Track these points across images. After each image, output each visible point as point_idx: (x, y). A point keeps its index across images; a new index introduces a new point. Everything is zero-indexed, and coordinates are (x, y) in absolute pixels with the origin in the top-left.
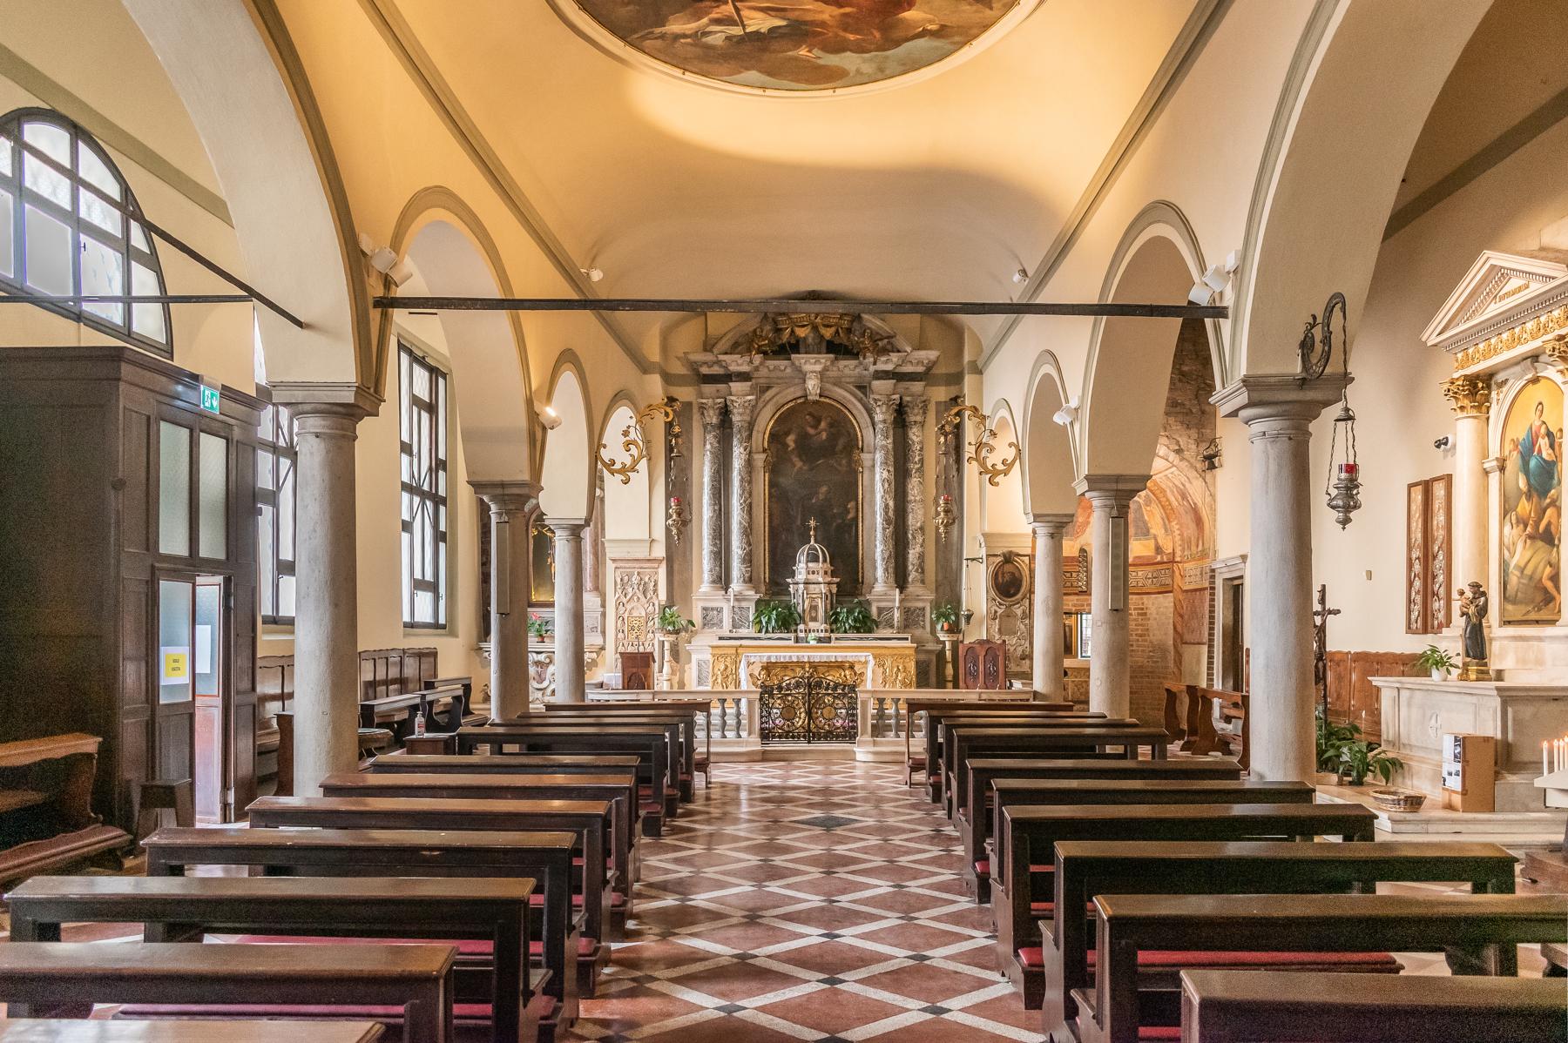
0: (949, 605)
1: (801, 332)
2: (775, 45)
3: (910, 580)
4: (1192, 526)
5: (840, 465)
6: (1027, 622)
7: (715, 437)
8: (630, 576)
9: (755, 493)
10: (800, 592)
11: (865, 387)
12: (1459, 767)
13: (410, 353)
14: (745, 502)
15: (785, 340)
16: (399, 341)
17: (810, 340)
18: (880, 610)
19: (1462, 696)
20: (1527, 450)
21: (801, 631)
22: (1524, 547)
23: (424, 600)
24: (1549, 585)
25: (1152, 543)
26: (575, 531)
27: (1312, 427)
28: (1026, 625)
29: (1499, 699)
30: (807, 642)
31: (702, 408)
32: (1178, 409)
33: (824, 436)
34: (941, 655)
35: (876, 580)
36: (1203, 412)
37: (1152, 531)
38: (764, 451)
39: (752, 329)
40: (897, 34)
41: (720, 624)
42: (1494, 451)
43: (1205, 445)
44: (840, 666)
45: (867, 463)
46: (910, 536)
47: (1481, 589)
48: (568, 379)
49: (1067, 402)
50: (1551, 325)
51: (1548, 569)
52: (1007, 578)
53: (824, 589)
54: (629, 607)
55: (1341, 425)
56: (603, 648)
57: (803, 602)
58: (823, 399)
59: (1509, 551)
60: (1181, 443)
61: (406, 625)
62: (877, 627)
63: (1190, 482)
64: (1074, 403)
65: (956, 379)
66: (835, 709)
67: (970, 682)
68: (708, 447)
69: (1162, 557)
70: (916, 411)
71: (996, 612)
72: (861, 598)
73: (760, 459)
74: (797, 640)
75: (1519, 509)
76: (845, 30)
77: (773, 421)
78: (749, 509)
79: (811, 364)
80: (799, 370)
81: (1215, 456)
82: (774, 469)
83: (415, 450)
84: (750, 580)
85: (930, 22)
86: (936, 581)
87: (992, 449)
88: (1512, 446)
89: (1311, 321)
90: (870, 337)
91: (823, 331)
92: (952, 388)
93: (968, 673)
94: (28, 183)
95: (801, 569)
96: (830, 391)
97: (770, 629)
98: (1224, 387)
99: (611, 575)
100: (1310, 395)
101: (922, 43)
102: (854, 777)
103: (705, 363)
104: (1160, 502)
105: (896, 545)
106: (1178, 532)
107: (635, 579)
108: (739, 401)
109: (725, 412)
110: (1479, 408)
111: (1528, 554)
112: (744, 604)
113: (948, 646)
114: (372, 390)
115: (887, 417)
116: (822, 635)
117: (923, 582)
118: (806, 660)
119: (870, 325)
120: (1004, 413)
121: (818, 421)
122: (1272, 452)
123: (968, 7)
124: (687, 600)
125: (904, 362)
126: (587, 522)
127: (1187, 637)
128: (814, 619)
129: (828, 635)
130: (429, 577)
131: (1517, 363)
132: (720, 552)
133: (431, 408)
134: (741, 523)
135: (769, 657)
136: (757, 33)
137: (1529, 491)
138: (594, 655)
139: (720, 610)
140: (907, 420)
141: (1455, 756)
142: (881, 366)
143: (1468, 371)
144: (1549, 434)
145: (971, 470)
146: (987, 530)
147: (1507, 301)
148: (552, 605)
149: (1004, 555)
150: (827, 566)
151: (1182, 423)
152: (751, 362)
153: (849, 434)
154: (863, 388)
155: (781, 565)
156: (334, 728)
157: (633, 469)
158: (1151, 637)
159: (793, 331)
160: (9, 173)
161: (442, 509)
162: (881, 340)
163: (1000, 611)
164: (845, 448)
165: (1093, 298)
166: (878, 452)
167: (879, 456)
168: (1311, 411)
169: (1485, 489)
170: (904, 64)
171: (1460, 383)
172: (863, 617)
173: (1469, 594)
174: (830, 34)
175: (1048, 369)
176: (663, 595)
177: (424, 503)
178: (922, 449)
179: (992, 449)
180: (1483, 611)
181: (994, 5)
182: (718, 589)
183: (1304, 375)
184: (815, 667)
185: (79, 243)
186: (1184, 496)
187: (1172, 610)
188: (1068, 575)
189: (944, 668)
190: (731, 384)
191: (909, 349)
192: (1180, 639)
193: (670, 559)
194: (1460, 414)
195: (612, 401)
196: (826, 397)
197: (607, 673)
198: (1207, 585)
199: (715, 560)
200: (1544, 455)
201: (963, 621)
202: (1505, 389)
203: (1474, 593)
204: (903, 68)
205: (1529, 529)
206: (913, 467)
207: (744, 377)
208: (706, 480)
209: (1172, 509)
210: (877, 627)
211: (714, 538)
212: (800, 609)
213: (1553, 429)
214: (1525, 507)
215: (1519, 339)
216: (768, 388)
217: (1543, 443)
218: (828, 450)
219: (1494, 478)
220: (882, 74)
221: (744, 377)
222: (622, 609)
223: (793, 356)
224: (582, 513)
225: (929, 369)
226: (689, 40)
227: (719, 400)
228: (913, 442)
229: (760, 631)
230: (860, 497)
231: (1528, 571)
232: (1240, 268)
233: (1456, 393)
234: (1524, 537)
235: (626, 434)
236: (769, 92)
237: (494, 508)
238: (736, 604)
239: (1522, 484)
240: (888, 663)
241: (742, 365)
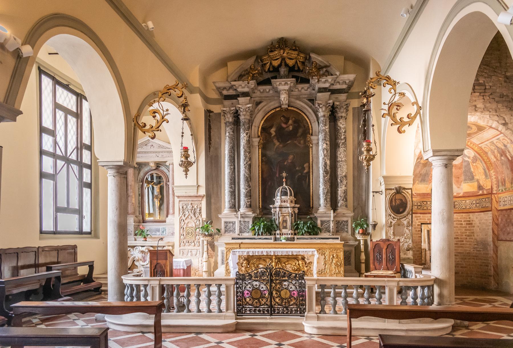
3: (339, 205)
5: (300, 143)
6: (410, 228)
7: (231, 129)
10: (277, 212)
11: (313, 100)
14: (247, 163)
18: (322, 222)
21: (278, 234)
25: (476, 184)
28: (409, 230)
30: (281, 241)
32: (504, 99)
33: (291, 128)
34: (358, 247)
35: (320, 205)
37: (476, 177)
38: (259, 137)
41: (234, 231)
44: (295, 258)
45: (314, 142)
52: (398, 202)
53: (290, 210)
54: (186, 222)
58: (290, 108)
60: (506, 119)
62: (321, 232)
66: (290, 291)
67: (377, 264)
68: (227, 134)
69: (483, 192)
70: (342, 110)
71: (391, 222)
72: (312, 216)
73: (256, 141)
74: (276, 239)
77: (263, 121)
78: (249, 167)
79: (282, 85)
82: (264, 147)
84: (250, 206)
86: (354, 206)
95: (278, 200)
96: (294, 103)
97: (260, 233)
103: (224, 88)
105: (331, 186)
106: (495, 177)
107: (190, 207)
108: (243, 107)
109: (236, 115)
112: (246, 220)
113: (362, 242)
115: (326, 114)
116: (289, 236)
117: (346, 206)
118: (272, 254)
121: (287, 120)
127: (502, 237)
128: (285, 228)
129: (292, 236)
132: (234, 191)
134: (245, 175)
135: (248, 252)
139: (234, 223)
140: (337, 116)
146: (385, 174)
149: (396, 189)
150: (292, 198)
153: (305, 126)
154: (312, 101)
158: (476, 236)
159: (271, 63)
163: (394, 222)
164: (302, 134)
166: (320, 133)
167: (321, 136)
172: (313, 226)
176: (204, 215)
178: (345, 132)
182: (232, 212)
184: (279, 259)
187: (491, 221)
188: (425, 203)
189: (360, 255)
191: (338, 73)
192: (497, 238)
193: (209, 196)
196: (292, 107)
199: (231, 195)
201: (371, 227)
206: (341, 142)
207: (245, 94)
208: (227, 152)
209: (491, 163)
210: (321, 232)
212: (277, 222)
216: (260, 102)
218: (293, 135)
221: (245, 94)
222: (183, 223)
227: (232, 108)
228: (340, 128)
229: (255, 235)
230: (311, 160)
238: (242, 220)
240: (327, 253)
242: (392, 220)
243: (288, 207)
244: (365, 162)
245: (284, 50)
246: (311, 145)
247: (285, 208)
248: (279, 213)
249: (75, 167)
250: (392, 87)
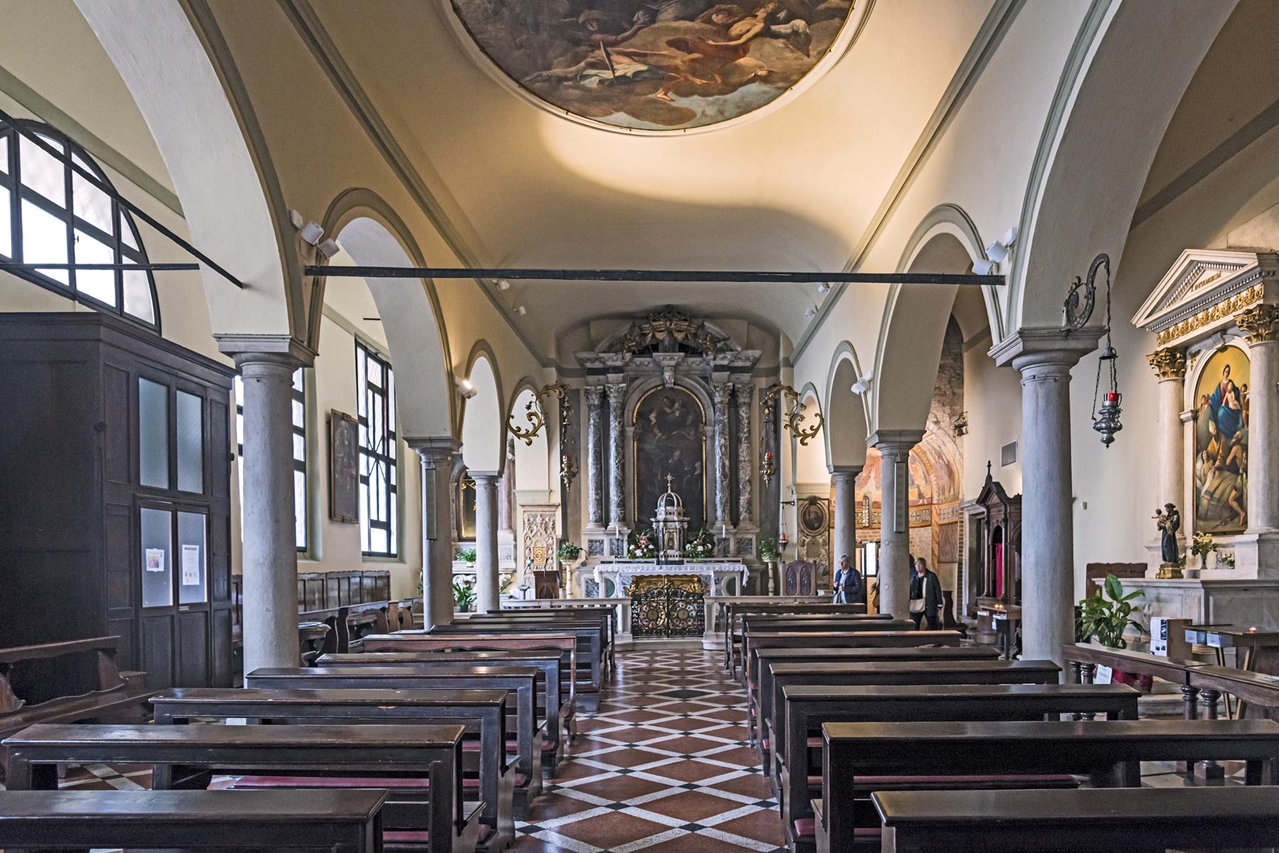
0: (772, 541)
1: (660, 336)
2: (639, 88)
3: (741, 518)
4: (946, 478)
5: (689, 435)
8: (535, 517)
9: (627, 456)
10: (661, 528)
12: (1165, 643)
13: (365, 349)
15: (648, 342)
16: (356, 340)
17: (667, 343)
19: (1170, 589)
20: (1216, 401)
22: (1213, 478)
23: (379, 535)
24: (1235, 504)
26: (492, 481)
27: (1072, 371)
29: (1203, 591)
31: (587, 392)
33: (677, 414)
35: (716, 519)
36: (954, 394)
37: (916, 482)
38: (633, 425)
39: (623, 334)
40: (735, 79)
42: (1189, 404)
43: (955, 418)
45: (709, 434)
46: (741, 487)
47: (1175, 509)
48: (482, 363)
49: (861, 375)
50: (1239, 303)
51: (1234, 493)
53: (677, 525)
55: (1106, 363)
56: (515, 571)
57: (663, 535)
58: (676, 387)
59: (1200, 480)
61: (364, 554)
63: (945, 445)
64: (867, 377)
65: (775, 371)
68: (592, 421)
70: (745, 395)
73: (630, 430)
75: (1209, 448)
76: (694, 75)
80: (658, 365)
81: (963, 426)
82: (640, 438)
84: (623, 520)
85: (761, 68)
87: (802, 418)
88: (1203, 401)
89: (1077, 281)
90: (711, 340)
91: (676, 335)
92: (771, 378)
93: (787, 584)
94: (25, 181)
98: (1001, 341)
99: (520, 515)
100: (1072, 344)
101: (754, 87)
102: (702, 661)
103: (588, 360)
104: (922, 461)
107: (539, 520)
109: (604, 396)
110: (1176, 373)
111: (1216, 483)
114: (305, 343)
117: (750, 520)
119: (710, 331)
120: (811, 393)
121: (673, 402)
122: (1041, 392)
123: (791, 55)
124: (578, 535)
125: (737, 358)
126: (501, 473)
128: (672, 548)
129: (681, 559)
130: (383, 518)
131: (1209, 337)
132: (601, 499)
133: (384, 393)
134: (616, 478)
136: (624, 76)
137: (1218, 433)
138: (509, 576)
141: (1162, 635)
142: (719, 362)
143: (1169, 345)
144: (1235, 389)
145: (786, 434)
147: (1201, 288)
148: (474, 540)
151: (939, 401)
152: (623, 358)
155: (647, 509)
156: (276, 623)
157: (534, 434)
159: (653, 335)
160: (6, 171)
161: (393, 468)
162: (719, 342)
163: (807, 540)
164: (693, 422)
165: (891, 270)
168: (1073, 358)
169: (1182, 435)
170: (739, 107)
171: (1163, 354)
173: (1165, 513)
174: (682, 79)
175: (847, 355)
177: (378, 463)
179: (802, 418)
180: (1177, 525)
181: (811, 53)
183: (1068, 327)
185: (73, 235)
186: (940, 456)
187: (930, 539)
189: (768, 582)
190: (609, 375)
191: (739, 349)
193: (564, 504)
194: (1162, 379)
195: (519, 383)
197: (519, 593)
200: (1231, 406)
202: (1198, 358)
203: (1169, 512)
204: (738, 110)
205: (1217, 463)
206: (743, 436)
207: (617, 370)
208: (591, 446)
209: (931, 466)
211: (597, 489)
213: (1239, 385)
214: (1213, 446)
215: (1212, 317)
216: (636, 378)
217: (1230, 396)
218: (680, 424)
219: (1189, 427)
220: (722, 116)
221: (617, 370)
222: (528, 542)
223: (654, 354)
224: (495, 467)
225: (754, 364)
226: (570, 83)
231: (1217, 495)
232: (1017, 243)
233: (1159, 362)
234: (1213, 469)
235: (529, 407)
236: (634, 132)
237: (423, 457)
239: (1212, 429)
241: (617, 360)
243: (675, 521)
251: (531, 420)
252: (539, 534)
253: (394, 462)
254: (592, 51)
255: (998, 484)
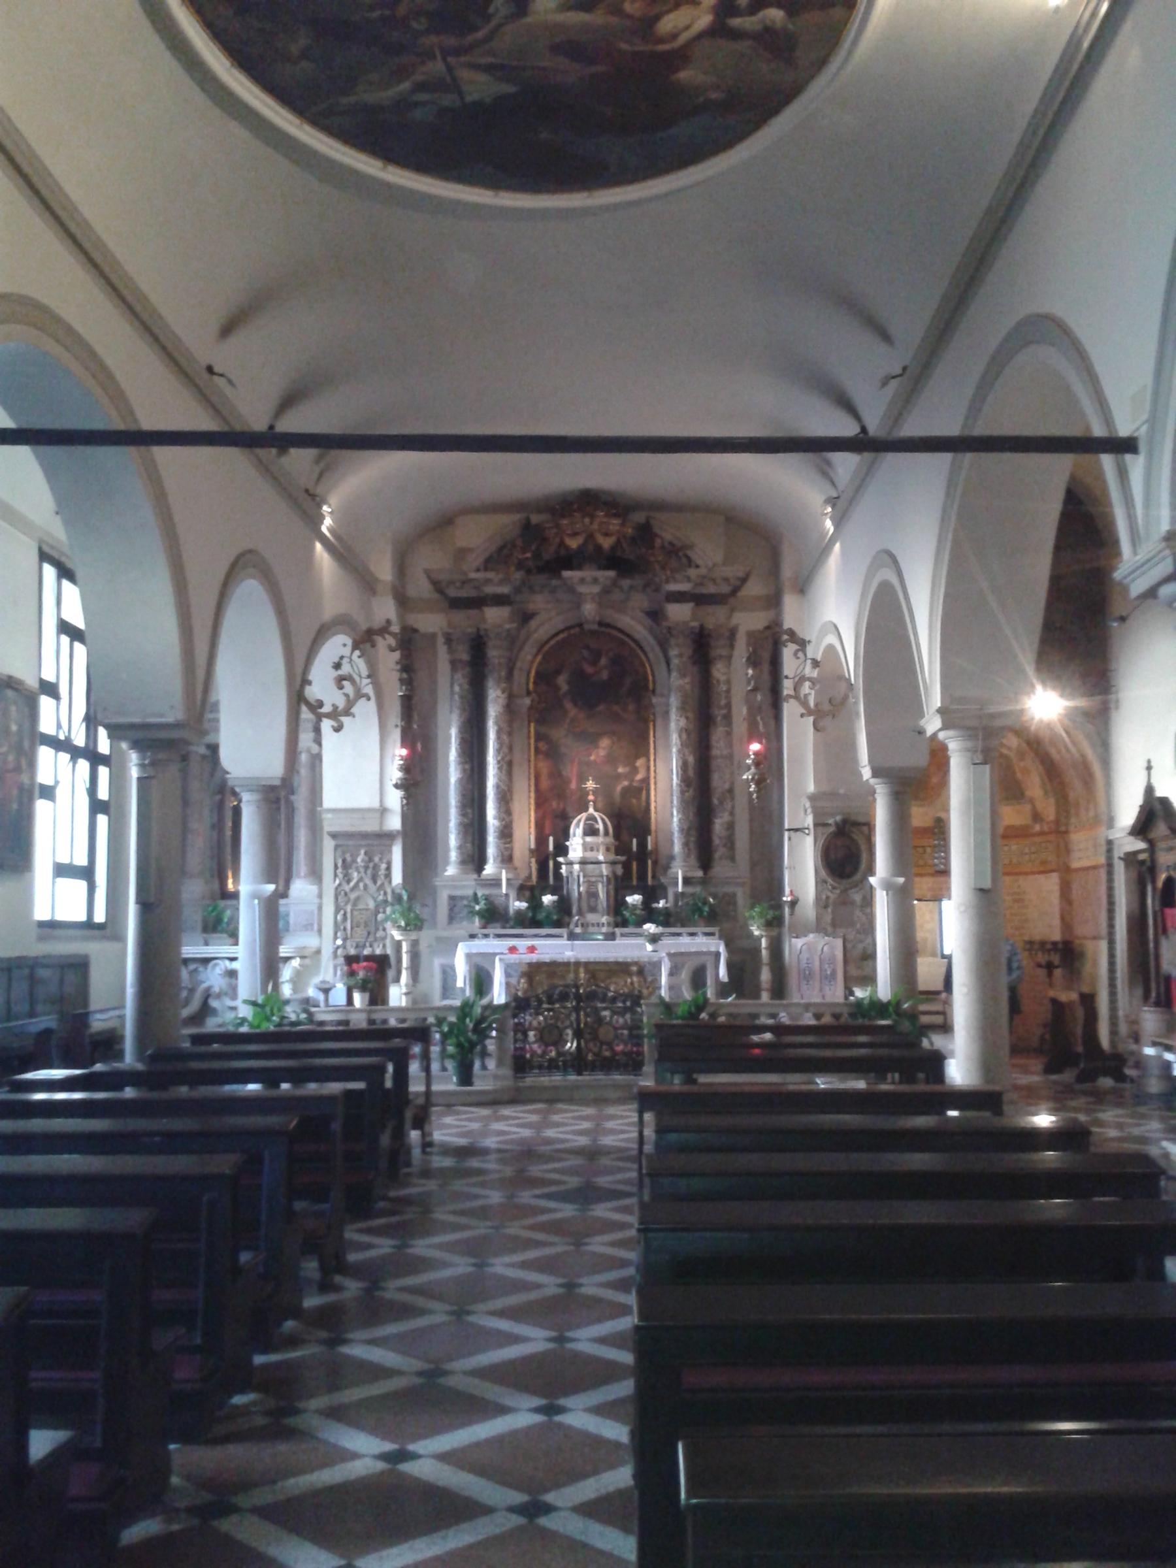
14: (503, 759)
25: (1027, 808)
33: (605, 675)
37: (1028, 793)
38: (529, 693)
65: (774, 601)
66: (616, 1029)
71: (828, 898)
77: (1151, 1424)
83: (63, 690)
95: (576, 846)
98: (1135, 553)
121: (597, 655)
128: (593, 910)
129: (611, 930)
161: (103, 772)
175: (888, 575)
198: (1102, 860)
206: (718, 714)
207: (499, 600)
228: (718, 681)
235: (337, 666)
242: (829, 894)
243: (598, 863)
244: (753, 786)
245: (592, 517)
246: (652, 717)
247: (592, 863)
248: (579, 876)
249: (84, 765)
250: (798, 647)
251: (341, 688)
252: (361, 885)
253: (105, 760)
254: (423, 63)
255: (1165, 802)
